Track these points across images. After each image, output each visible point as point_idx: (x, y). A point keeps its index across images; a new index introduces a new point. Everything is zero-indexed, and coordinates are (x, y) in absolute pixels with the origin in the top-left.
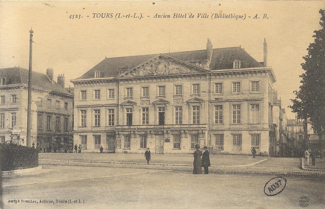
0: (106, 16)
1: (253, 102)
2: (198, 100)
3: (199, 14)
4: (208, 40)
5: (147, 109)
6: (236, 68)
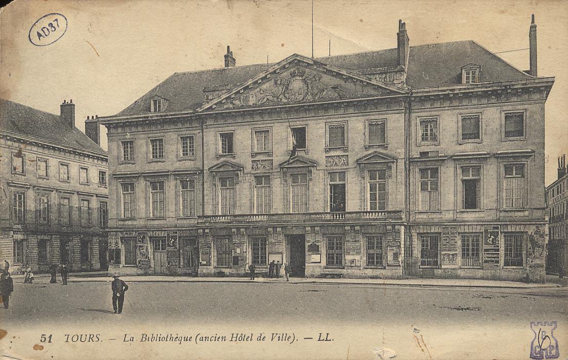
0: (88, 339)
1: (127, 181)
2: (384, 159)
3: (273, 334)
5: (343, 174)
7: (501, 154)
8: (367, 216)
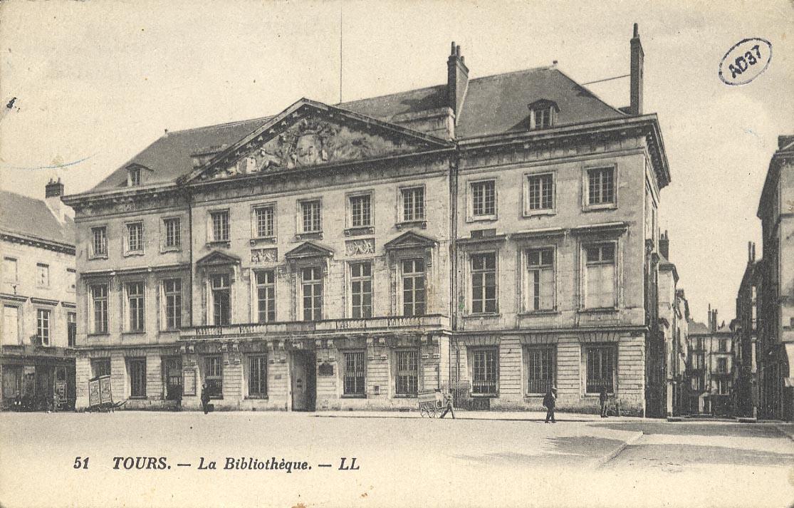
4: (453, 48)
5: (367, 266)
6: (538, 128)
7: (90, 273)
8: (256, 329)
